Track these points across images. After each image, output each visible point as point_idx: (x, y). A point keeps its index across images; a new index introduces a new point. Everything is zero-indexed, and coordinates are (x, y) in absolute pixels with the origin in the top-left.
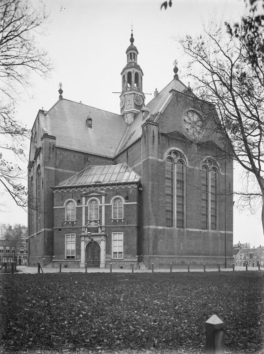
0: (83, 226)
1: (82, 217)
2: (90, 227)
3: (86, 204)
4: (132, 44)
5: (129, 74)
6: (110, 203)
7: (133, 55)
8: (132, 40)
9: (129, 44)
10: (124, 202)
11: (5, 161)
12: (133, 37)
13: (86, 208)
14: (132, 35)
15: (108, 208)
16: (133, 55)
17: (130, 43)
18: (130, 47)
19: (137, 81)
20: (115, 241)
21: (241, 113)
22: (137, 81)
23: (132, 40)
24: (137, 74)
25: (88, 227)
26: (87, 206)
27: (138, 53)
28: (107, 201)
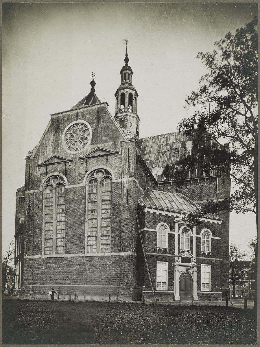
0: (176, 255)
1: (175, 245)
2: (184, 256)
3: (178, 232)
4: (127, 64)
5: (123, 95)
6: (200, 234)
7: (127, 75)
8: (127, 60)
9: (124, 64)
10: (211, 236)
11: (245, 168)
12: (128, 57)
13: (179, 236)
14: (127, 55)
15: (198, 240)
16: (127, 75)
17: (125, 63)
18: (124, 67)
19: (130, 103)
20: (208, 283)
21: (60, 161)
22: (130, 103)
23: (127, 60)
24: (131, 95)
25: (182, 256)
26: (179, 233)
27: (132, 73)
28: (198, 232)
